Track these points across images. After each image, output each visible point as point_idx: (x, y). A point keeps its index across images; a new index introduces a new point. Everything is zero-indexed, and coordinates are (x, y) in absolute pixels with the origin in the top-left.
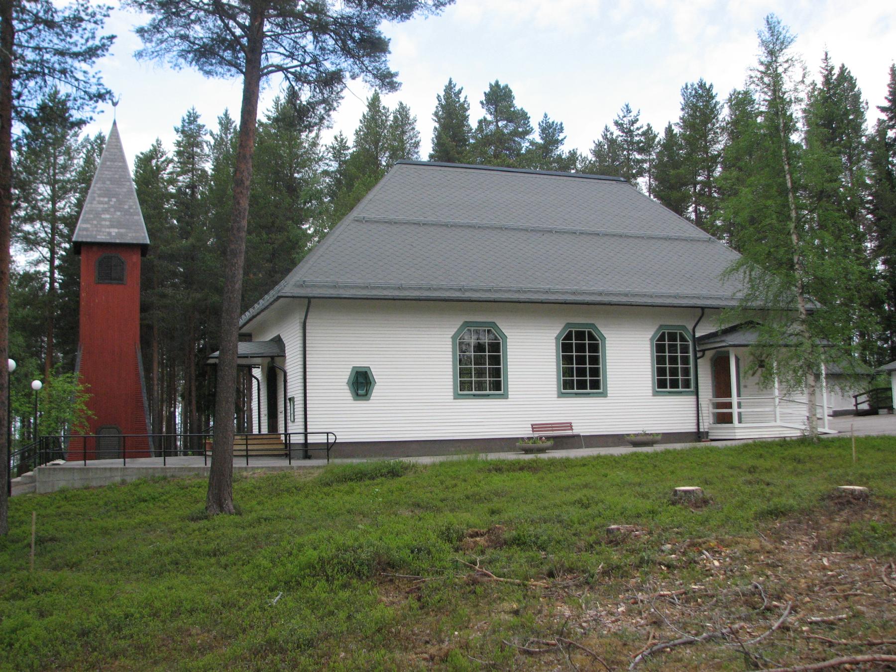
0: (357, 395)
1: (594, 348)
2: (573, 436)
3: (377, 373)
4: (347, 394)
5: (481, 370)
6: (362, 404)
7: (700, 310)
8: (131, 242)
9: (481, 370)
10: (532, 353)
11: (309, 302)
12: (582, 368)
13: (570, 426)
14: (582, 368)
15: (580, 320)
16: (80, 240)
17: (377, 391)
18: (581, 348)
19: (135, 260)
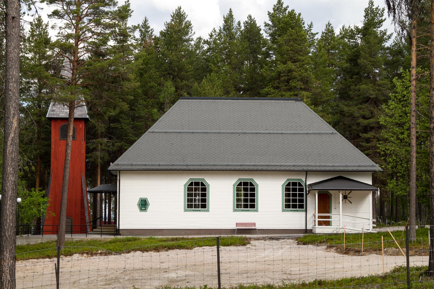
0: (141, 209)
1: (253, 189)
2: (255, 229)
3: (150, 201)
4: (137, 209)
5: (197, 197)
6: (143, 213)
7: (305, 172)
8: (78, 117)
9: (197, 197)
10: (222, 190)
11: (119, 172)
12: (247, 197)
13: (254, 224)
14: (247, 197)
15: (246, 177)
16: (50, 117)
17: (150, 208)
18: (246, 190)
19: (81, 127)
